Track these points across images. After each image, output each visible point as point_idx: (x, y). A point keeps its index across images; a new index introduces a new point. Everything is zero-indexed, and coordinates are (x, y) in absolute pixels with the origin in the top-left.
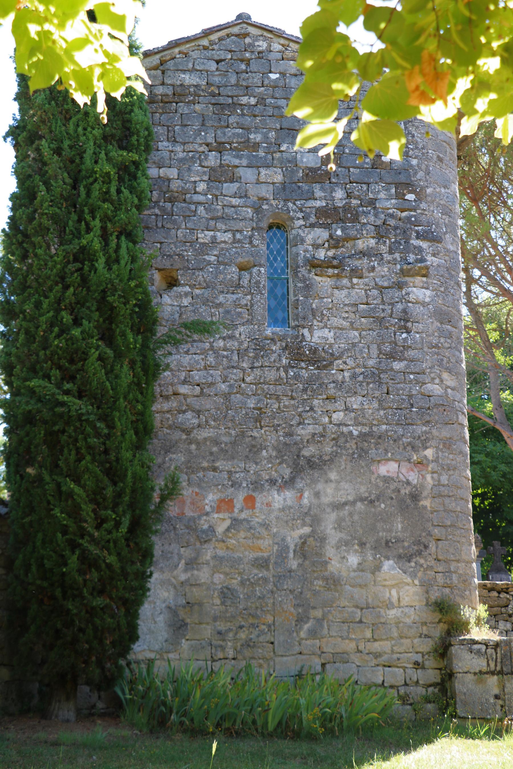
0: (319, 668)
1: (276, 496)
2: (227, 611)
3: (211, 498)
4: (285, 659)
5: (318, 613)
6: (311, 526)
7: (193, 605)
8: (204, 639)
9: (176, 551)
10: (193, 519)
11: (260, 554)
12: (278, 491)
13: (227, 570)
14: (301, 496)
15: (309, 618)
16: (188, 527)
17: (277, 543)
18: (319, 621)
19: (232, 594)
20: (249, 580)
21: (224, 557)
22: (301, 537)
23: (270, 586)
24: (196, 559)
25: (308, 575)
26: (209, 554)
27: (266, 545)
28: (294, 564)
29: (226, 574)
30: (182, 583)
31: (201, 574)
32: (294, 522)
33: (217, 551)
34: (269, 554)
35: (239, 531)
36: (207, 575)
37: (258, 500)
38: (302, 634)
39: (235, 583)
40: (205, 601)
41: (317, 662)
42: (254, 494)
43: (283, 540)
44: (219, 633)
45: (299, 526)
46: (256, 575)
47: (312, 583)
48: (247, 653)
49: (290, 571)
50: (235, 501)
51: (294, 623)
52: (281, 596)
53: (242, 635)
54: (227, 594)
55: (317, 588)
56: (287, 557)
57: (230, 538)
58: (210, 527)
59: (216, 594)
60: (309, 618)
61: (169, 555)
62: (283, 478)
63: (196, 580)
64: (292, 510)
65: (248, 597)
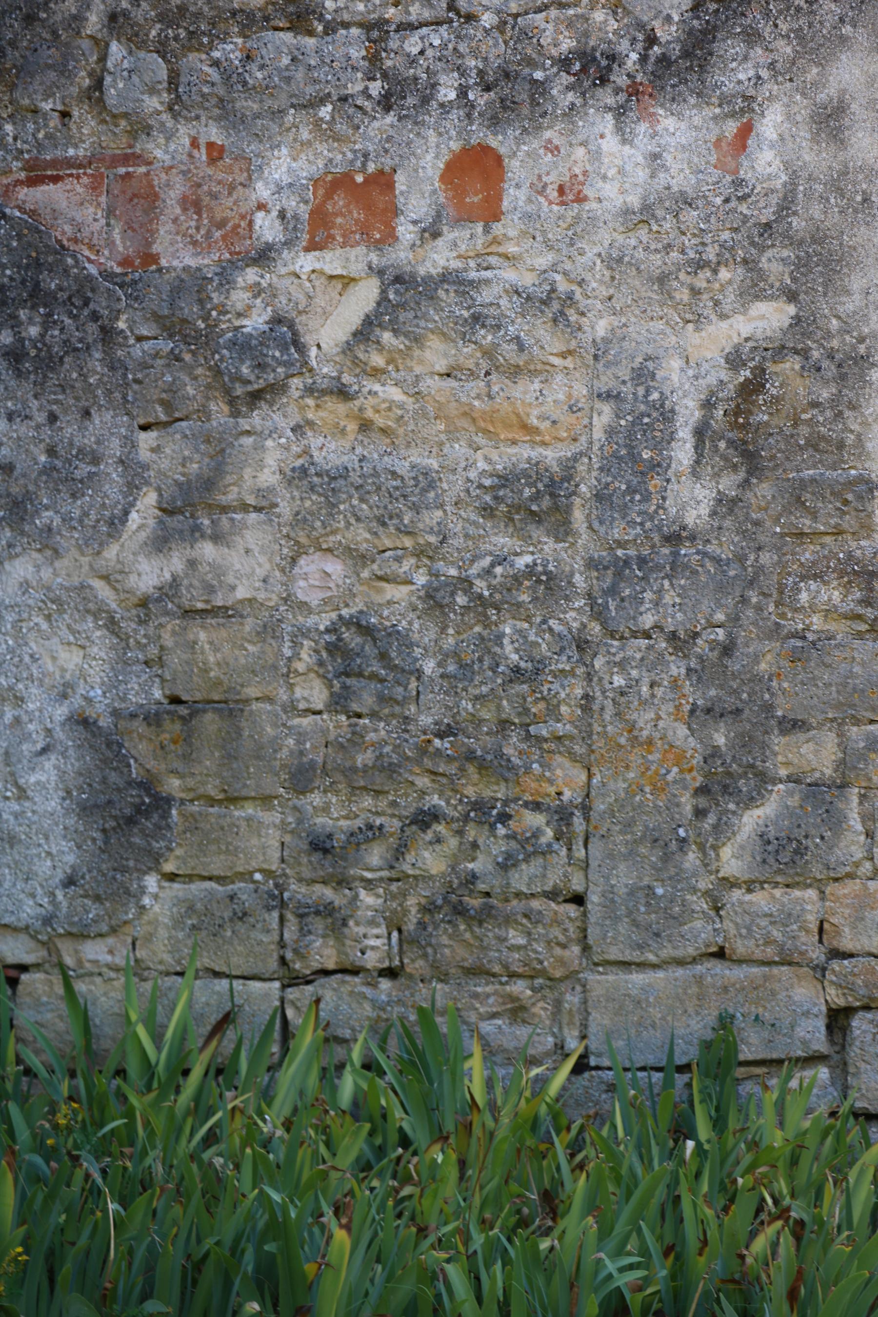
0: (813, 1033)
1: (610, 144)
2: (356, 739)
3: (286, 170)
4: (638, 978)
5: (818, 754)
6: (792, 297)
7: (197, 709)
8: (247, 876)
9: (115, 447)
10: (195, 285)
11: (524, 453)
12: (620, 112)
13: (360, 536)
14: (746, 131)
15: (764, 779)
16: (173, 326)
17: (608, 396)
18: (821, 794)
19: (383, 656)
20: (465, 584)
21: (344, 473)
22: (734, 361)
23: (573, 616)
24: (209, 484)
25: (767, 558)
26: (272, 458)
27: (557, 412)
28: (692, 499)
29: (358, 558)
30: (144, 603)
31: (233, 559)
32: (701, 280)
33: (314, 441)
34: (567, 451)
35: (418, 340)
36: (262, 565)
37: (515, 169)
38: (731, 861)
39: (396, 602)
40: (252, 692)
41: (804, 1003)
42: (493, 142)
43: (643, 375)
44: (320, 846)
45: (729, 299)
46: (501, 560)
47: (785, 598)
48: (451, 945)
49: (674, 539)
50: (401, 181)
51: (687, 803)
52: (622, 665)
53: (431, 860)
54: (357, 654)
55: (817, 622)
56: (656, 466)
57: (376, 373)
58: (277, 320)
59: (307, 657)
60: (764, 779)
61: (84, 469)
62: (652, 40)
63: (210, 589)
64: (691, 216)
65: (461, 672)
